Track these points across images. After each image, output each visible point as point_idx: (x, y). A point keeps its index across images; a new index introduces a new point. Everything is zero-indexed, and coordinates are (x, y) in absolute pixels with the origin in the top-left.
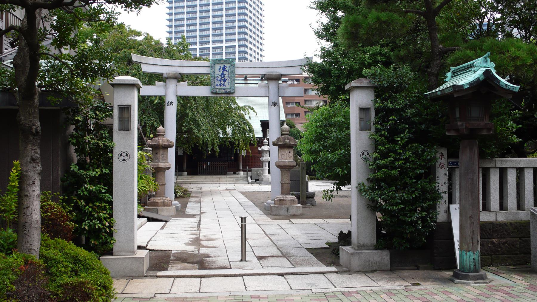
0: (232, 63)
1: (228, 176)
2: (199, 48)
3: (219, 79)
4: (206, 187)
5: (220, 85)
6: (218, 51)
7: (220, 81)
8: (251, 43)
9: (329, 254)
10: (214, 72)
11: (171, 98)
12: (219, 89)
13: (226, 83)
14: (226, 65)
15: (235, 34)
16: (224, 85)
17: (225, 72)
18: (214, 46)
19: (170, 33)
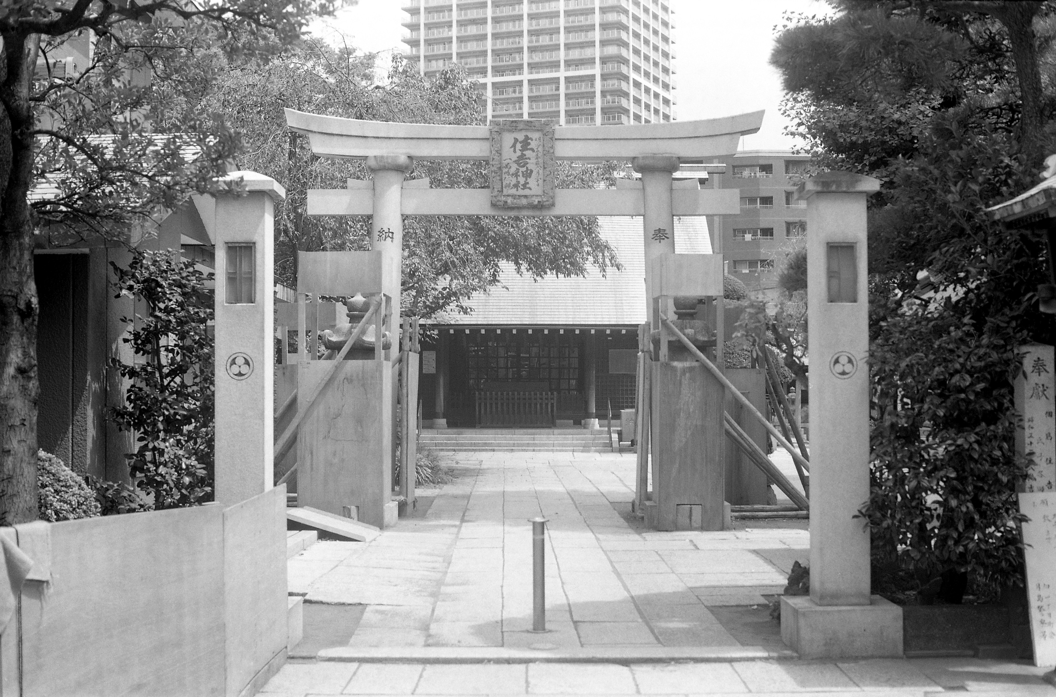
0: (547, 129)
1: (556, 431)
2: (493, 84)
3: (513, 170)
4: (486, 459)
5: (516, 186)
6: (546, 90)
7: (516, 175)
8: (637, 68)
9: (760, 622)
10: (499, 152)
11: (390, 216)
12: (514, 196)
13: (532, 182)
14: (530, 135)
15: (592, 44)
16: (525, 186)
17: (528, 153)
18: (535, 76)
19: (414, 43)
